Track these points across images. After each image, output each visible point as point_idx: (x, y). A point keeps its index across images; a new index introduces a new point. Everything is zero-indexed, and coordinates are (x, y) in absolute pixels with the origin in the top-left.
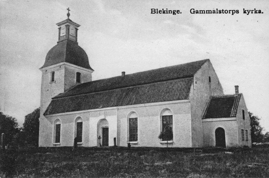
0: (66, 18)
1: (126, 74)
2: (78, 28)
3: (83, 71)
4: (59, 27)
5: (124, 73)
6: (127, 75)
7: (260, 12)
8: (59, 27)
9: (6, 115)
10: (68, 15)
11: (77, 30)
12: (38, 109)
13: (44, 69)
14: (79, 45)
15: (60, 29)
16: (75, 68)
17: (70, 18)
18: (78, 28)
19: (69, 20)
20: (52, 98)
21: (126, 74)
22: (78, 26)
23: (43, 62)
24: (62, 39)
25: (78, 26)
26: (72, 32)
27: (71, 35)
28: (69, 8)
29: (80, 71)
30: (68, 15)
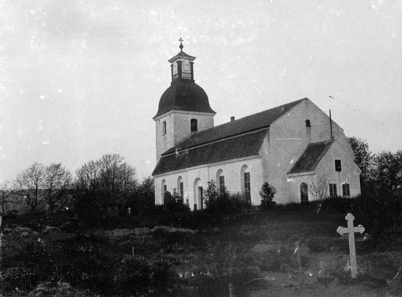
0: (179, 50)
1: (236, 119)
2: (194, 61)
3: (202, 120)
4: (171, 64)
5: (233, 118)
6: (239, 121)
7: (180, 40)
8: (171, 64)
9: (238, 193)
10: (181, 47)
11: (192, 64)
12: (264, 186)
13: (157, 118)
14: (170, 85)
15: (172, 66)
16: (187, 117)
17: (184, 50)
18: (194, 61)
19: (182, 54)
20: (162, 155)
21: (236, 119)
22: (194, 58)
23: (156, 109)
24: (174, 78)
25: (194, 58)
26: (186, 68)
27: (184, 72)
28: (181, 38)
29: (194, 117)
30: (181, 47)
